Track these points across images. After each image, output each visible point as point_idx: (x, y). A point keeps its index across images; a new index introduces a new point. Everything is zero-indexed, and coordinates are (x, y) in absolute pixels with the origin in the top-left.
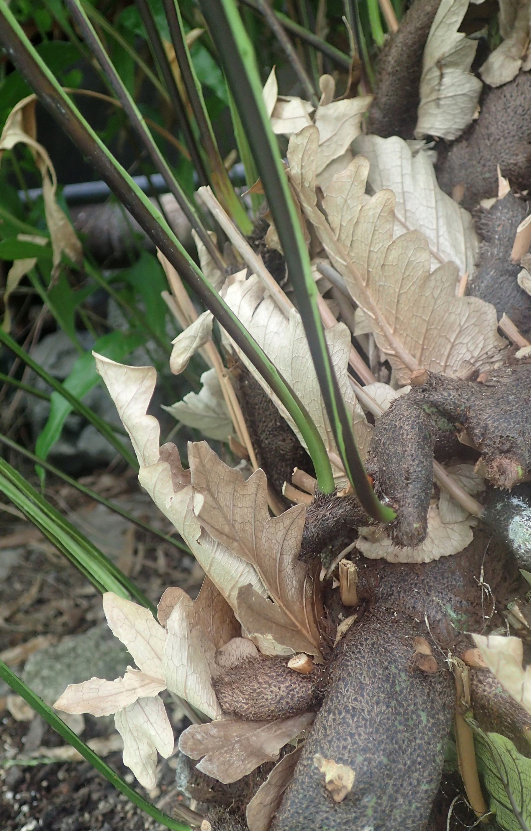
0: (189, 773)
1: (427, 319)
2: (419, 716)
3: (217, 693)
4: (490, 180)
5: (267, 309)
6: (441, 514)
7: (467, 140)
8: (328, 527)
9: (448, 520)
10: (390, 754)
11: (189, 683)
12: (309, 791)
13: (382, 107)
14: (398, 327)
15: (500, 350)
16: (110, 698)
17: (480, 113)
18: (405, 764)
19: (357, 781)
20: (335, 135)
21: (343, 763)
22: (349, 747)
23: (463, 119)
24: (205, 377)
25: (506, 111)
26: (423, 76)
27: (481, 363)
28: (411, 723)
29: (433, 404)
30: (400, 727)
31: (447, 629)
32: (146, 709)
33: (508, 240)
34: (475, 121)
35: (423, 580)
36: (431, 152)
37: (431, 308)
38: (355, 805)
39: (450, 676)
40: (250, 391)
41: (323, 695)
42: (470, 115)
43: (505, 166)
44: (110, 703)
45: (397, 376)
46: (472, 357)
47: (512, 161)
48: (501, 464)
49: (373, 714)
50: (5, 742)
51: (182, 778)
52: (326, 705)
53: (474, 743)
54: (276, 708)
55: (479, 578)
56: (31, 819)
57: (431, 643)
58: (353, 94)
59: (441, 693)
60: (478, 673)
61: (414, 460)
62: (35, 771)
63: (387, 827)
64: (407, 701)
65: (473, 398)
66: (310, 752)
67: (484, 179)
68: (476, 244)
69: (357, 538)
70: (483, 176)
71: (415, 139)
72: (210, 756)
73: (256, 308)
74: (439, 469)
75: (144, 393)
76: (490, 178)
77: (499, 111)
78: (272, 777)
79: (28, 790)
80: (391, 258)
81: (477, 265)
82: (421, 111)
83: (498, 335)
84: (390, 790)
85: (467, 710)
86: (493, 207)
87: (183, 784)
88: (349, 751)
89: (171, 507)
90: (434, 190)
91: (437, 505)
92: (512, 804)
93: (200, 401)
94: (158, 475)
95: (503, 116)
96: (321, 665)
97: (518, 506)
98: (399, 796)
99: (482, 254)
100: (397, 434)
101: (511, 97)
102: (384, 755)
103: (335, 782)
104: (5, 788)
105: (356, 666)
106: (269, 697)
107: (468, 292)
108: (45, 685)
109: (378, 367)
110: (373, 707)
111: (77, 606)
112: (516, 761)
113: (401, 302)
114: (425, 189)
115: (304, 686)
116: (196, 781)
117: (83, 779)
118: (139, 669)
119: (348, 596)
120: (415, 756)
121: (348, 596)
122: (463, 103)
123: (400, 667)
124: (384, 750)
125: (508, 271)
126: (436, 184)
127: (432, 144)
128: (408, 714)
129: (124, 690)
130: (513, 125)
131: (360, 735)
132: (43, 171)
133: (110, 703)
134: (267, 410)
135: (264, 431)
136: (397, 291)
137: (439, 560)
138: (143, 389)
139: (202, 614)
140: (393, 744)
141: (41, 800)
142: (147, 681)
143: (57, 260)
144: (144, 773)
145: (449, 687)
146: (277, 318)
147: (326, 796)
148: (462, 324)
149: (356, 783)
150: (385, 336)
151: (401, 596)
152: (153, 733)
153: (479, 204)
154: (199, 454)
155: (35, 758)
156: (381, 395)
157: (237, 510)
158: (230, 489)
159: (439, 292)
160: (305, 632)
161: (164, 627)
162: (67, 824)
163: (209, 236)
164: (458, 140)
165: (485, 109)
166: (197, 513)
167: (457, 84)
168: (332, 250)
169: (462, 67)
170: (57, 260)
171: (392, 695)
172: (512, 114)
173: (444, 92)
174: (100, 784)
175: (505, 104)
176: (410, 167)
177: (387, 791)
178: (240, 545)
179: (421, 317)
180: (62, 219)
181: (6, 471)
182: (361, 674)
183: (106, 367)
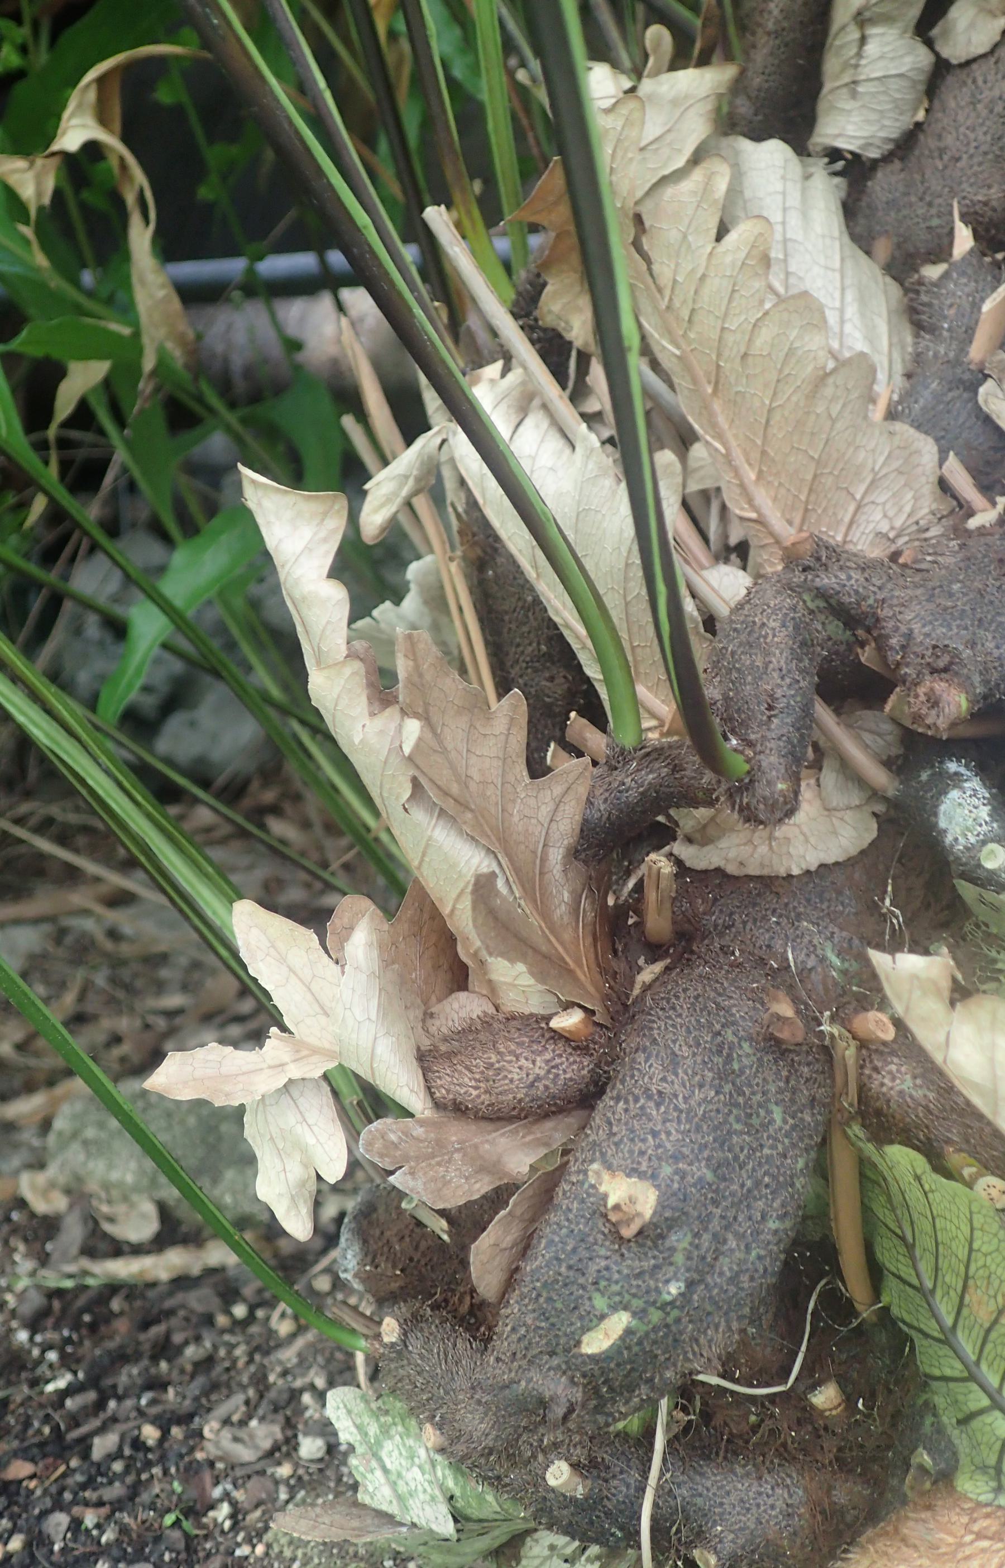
0: (361, 1249)
1: (816, 456)
2: (769, 1112)
3: (426, 1071)
4: (939, 231)
5: (537, 426)
6: (824, 794)
7: (902, 159)
8: (627, 804)
9: (834, 804)
10: (719, 1167)
11: (379, 1051)
12: (578, 1224)
13: (754, 94)
14: (765, 469)
15: (940, 519)
16: (240, 1078)
17: (927, 111)
18: (743, 1186)
19: (661, 1205)
20: (669, 131)
21: (639, 1177)
22: (650, 1152)
23: (897, 120)
24: (414, 570)
25: (975, 109)
26: (830, 40)
27: (906, 539)
28: (755, 1121)
29: (820, 594)
30: (738, 1127)
31: (824, 984)
32: (301, 1101)
33: (966, 332)
34: (918, 125)
35: (787, 905)
36: (837, 180)
37: (824, 436)
38: (656, 1246)
39: (827, 1052)
40: (496, 588)
41: (609, 1078)
42: (909, 114)
43: (967, 206)
44: (241, 1086)
45: (759, 560)
46: (892, 528)
47: (980, 198)
48: (932, 689)
49: (693, 1103)
50: (15, 1250)
51: (349, 1257)
52: (613, 1088)
53: (860, 1182)
54: (526, 1095)
55: (883, 900)
56: (63, 1370)
57: (796, 1000)
58: (704, 61)
59: (807, 1080)
60: (873, 1056)
61: (782, 678)
62: (69, 1297)
63: (707, 1286)
64: (750, 1086)
65: (890, 586)
66: (584, 1161)
67: (928, 228)
68: (909, 339)
69: (675, 839)
70: (928, 224)
71: (809, 155)
72: (411, 1168)
73: (514, 432)
74: (823, 712)
75: (325, 540)
76: (941, 227)
77: (962, 108)
78: (515, 1205)
79: (57, 1327)
80: (758, 342)
81: (908, 376)
82: (822, 106)
83: (938, 491)
84: (715, 1225)
85: (852, 1118)
86: (946, 275)
87: (350, 1266)
88: (650, 1159)
89: (362, 741)
90: (840, 239)
91: (818, 780)
92: (918, 1275)
93: (401, 618)
94: (342, 682)
95: (968, 117)
96: (607, 1028)
97: (956, 774)
98: (730, 1236)
99: (918, 355)
100: (756, 635)
101: (985, 82)
102: (708, 1166)
103: (624, 1207)
104: (14, 1324)
105: (666, 1029)
106: (516, 1077)
107: (891, 415)
108: (89, 1155)
109: (724, 554)
110: (693, 1092)
111: (147, 1026)
112: (930, 1195)
113: (772, 423)
114: (823, 236)
115: (575, 1062)
116: (373, 1261)
117: (155, 1311)
118: (291, 1033)
119: (658, 922)
120: (760, 1173)
121: (658, 922)
122: (898, 91)
123: (742, 1033)
124: (708, 1159)
125: (961, 381)
126: (844, 228)
127: (840, 165)
128: (751, 1107)
129: (265, 1066)
130: (985, 133)
131: (668, 1134)
132: (130, 199)
133: (241, 1086)
134: (525, 624)
135: (517, 661)
136: (767, 402)
137: (816, 871)
138: (322, 534)
139: (402, 946)
140: (723, 1151)
141: (81, 1343)
142: (305, 1053)
143: (148, 364)
144: (293, 1213)
145: (823, 1072)
146: (555, 443)
147: (606, 1231)
148: (877, 468)
149: (659, 1209)
150: (742, 486)
151: (748, 928)
152: (311, 1141)
153: (917, 271)
154: (414, 654)
155: (70, 1276)
156: (726, 585)
157: (474, 759)
158: (463, 722)
159: (839, 407)
160: (579, 973)
161: (337, 963)
162: (130, 1376)
163: (436, 309)
164: (887, 158)
165: (936, 103)
166: (407, 750)
167: (891, 55)
168: (656, 330)
169: (899, 24)
170: (148, 364)
171: (724, 1075)
172: (984, 113)
173: (866, 70)
174: (187, 1319)
175: (973, 95)
176: (797, 195)
177: (710, 1227)
178: (476, 817)
179: (806, 451)
180: (163, 286)
181: (60, 707)
182: (674, 1042)
183: (260, 493)
